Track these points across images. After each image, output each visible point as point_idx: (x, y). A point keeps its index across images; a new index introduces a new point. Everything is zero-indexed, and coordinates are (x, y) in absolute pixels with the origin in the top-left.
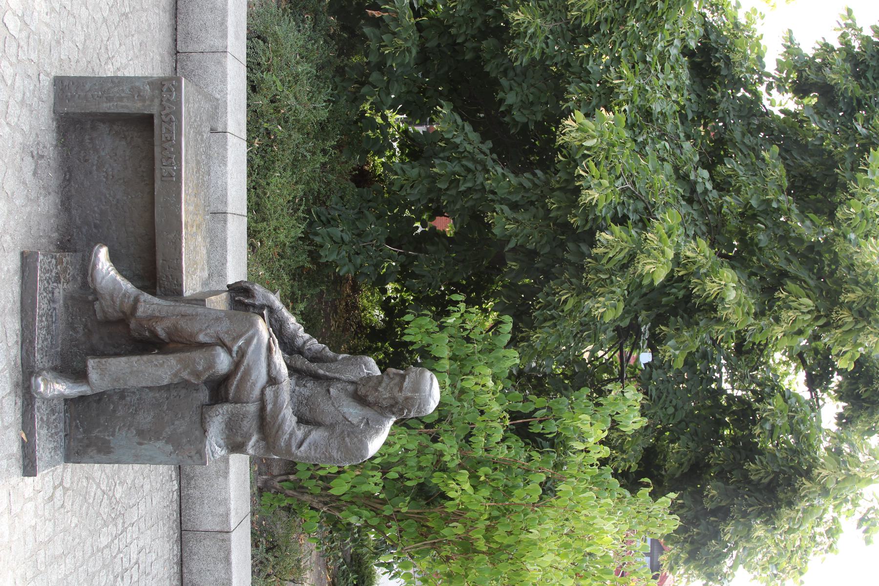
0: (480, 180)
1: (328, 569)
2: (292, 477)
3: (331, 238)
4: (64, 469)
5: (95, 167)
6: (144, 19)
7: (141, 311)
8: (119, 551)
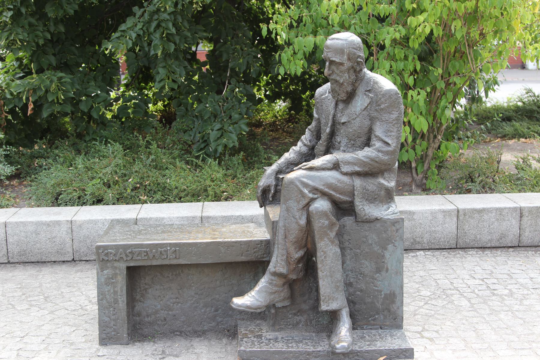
0: (165, 16)
1: (490, 141)
2: (414, 165)
3: (218, 138)
4: (407, 331)
5: (170, 313)
6: (48, 285)
7: (283, 270)
8: (473, 292)
